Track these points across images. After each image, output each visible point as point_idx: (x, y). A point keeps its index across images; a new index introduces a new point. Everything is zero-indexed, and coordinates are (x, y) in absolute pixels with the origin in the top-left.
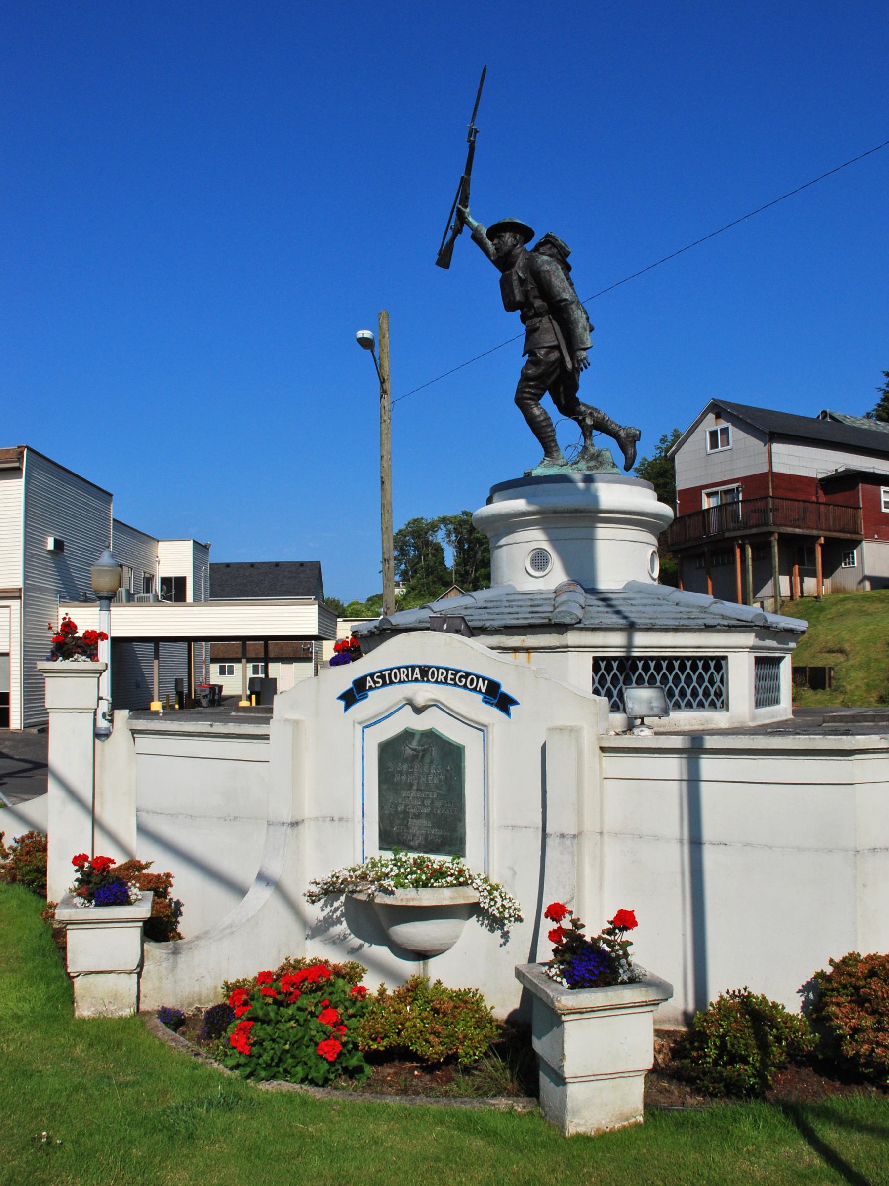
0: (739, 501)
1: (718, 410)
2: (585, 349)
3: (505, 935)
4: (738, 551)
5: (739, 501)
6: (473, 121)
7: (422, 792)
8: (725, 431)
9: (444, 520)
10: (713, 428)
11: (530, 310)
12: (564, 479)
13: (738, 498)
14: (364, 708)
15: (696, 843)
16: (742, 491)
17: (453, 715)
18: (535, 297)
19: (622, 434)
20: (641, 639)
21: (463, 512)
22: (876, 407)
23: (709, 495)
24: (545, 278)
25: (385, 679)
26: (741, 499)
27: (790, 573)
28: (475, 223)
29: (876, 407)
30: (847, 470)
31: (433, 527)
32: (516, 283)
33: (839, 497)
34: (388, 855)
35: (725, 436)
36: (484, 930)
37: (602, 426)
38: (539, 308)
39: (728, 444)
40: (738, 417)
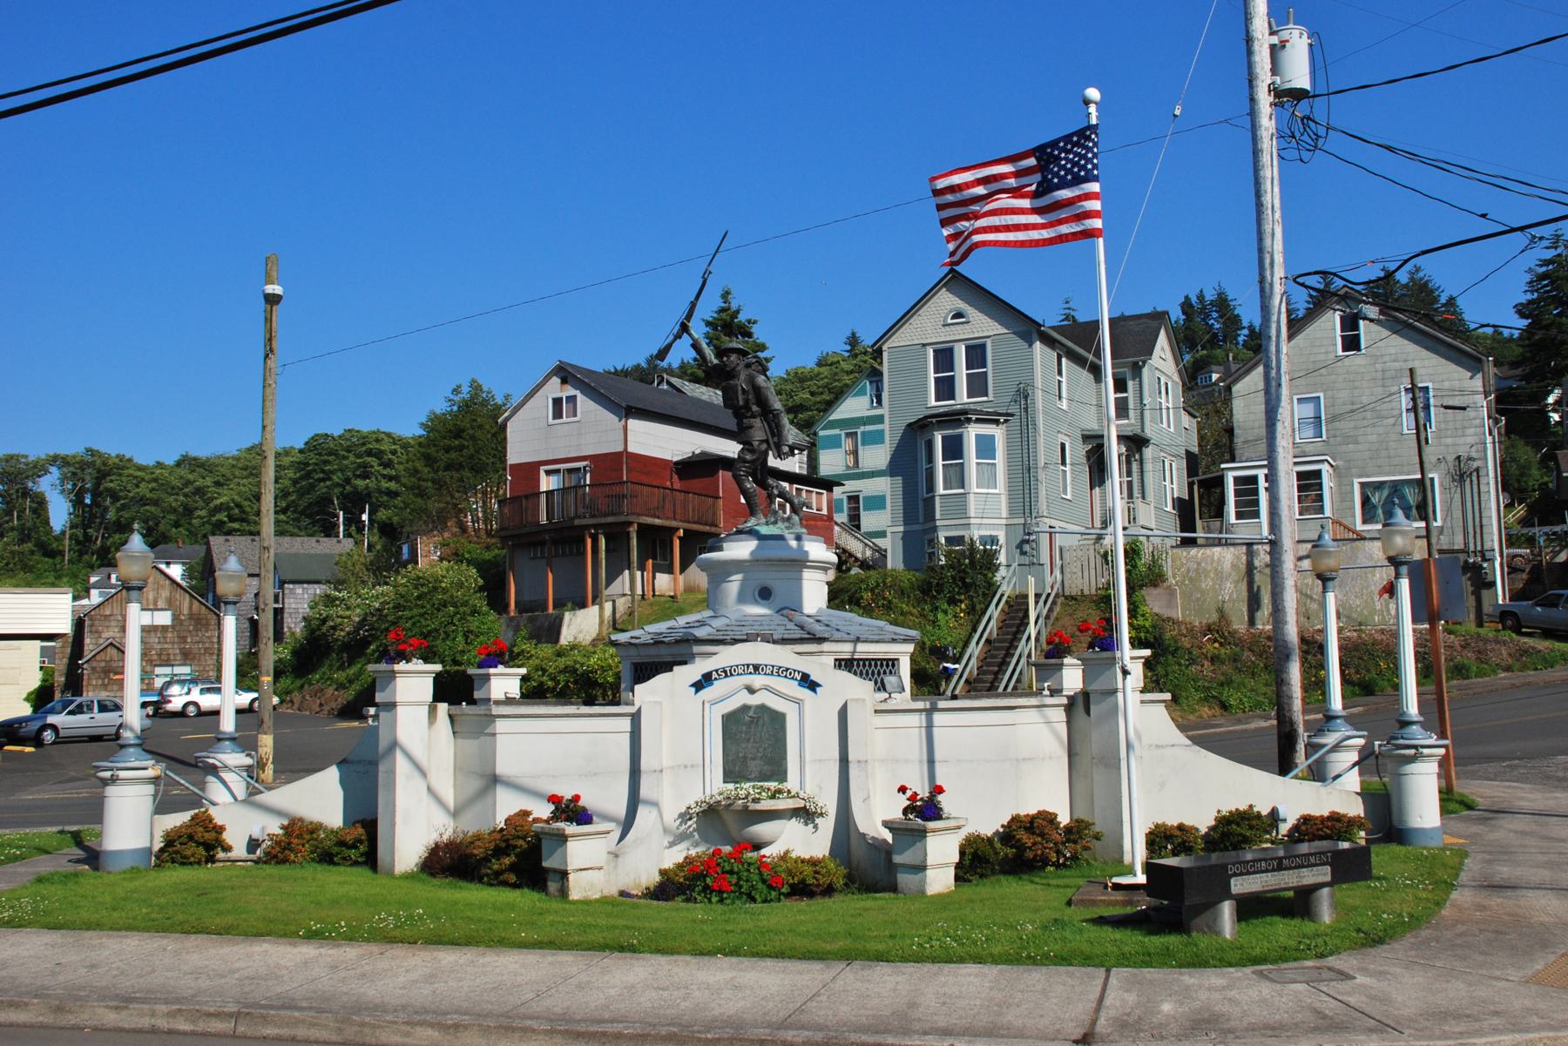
1: (565, 374)
3: (816, 827)
4: (589, 541)
7: (754, 742)
8: (572, 399)
9: (54, 460)
12: (781, 538)
14: (707, 693)
15: (931, 762)
17: (776, 695)
20: (861, 647)
21: (88, 450)
23: (548, 473)
25: (727, 673)
27: (642, 568)
30: (703, 453)
31: (39, 469)
33: (697, 484)
34: (731, 786)
36: (801, 825)
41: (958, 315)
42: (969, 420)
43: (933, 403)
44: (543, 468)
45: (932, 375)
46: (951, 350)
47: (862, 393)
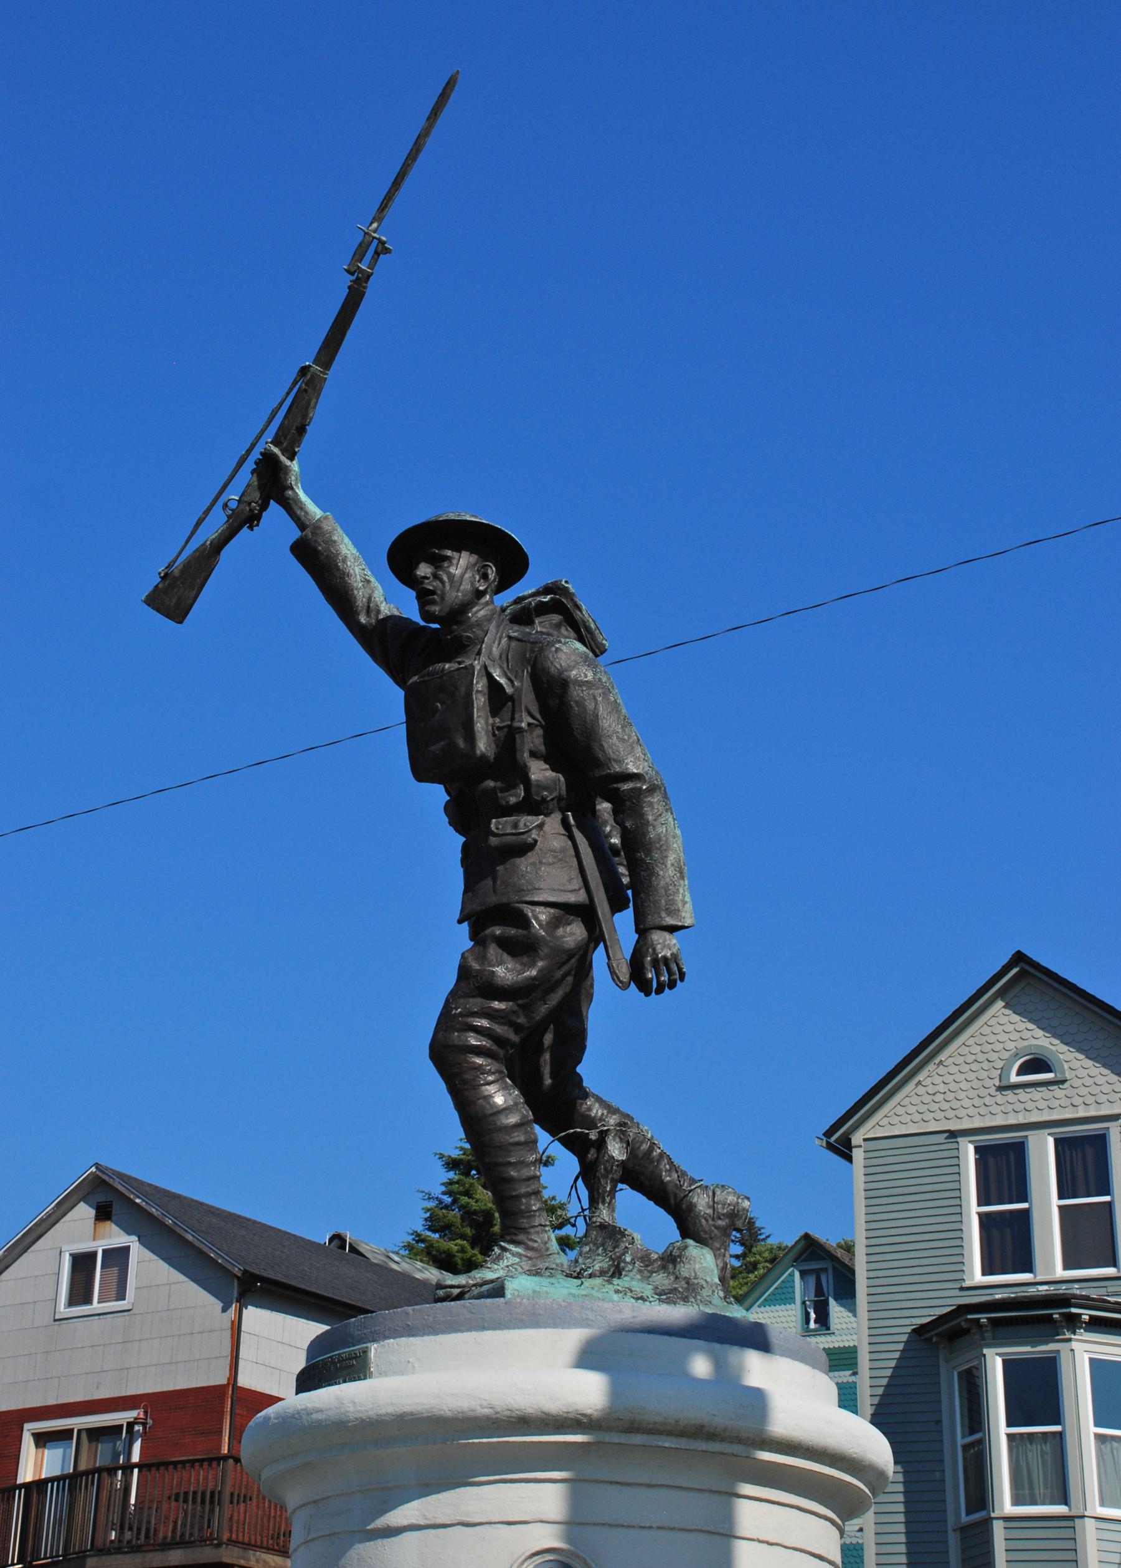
0: (128, 1468)
1: (107, 1197)
2: (673, 929)
5: (128, 1468)
6: (379, 216)
8: (117, 1257)
10: (84, 1246)
11: (510, 787)
13: (129, 1454)
16: (144, 1435)
18: (534, 754)
19: (701, 1202)
22: (410, 1239)
23: (42, 1440)
24: (580, 704)
26: (136, 1458)
28: (314, 510)
29: (410, 1239)
32: (480, 701)
35: (115, 1271)
37: (645, 1175)
38: (541, 786)
39: (121, 1296)
40: (162, 1224)
41: (1036, 1064)
42: (1073, 1322)
43: (977, 1276)
44: (30, 1428)
45: (973, 1210)
46: (1019, 1150)
47: (784, 1297)
